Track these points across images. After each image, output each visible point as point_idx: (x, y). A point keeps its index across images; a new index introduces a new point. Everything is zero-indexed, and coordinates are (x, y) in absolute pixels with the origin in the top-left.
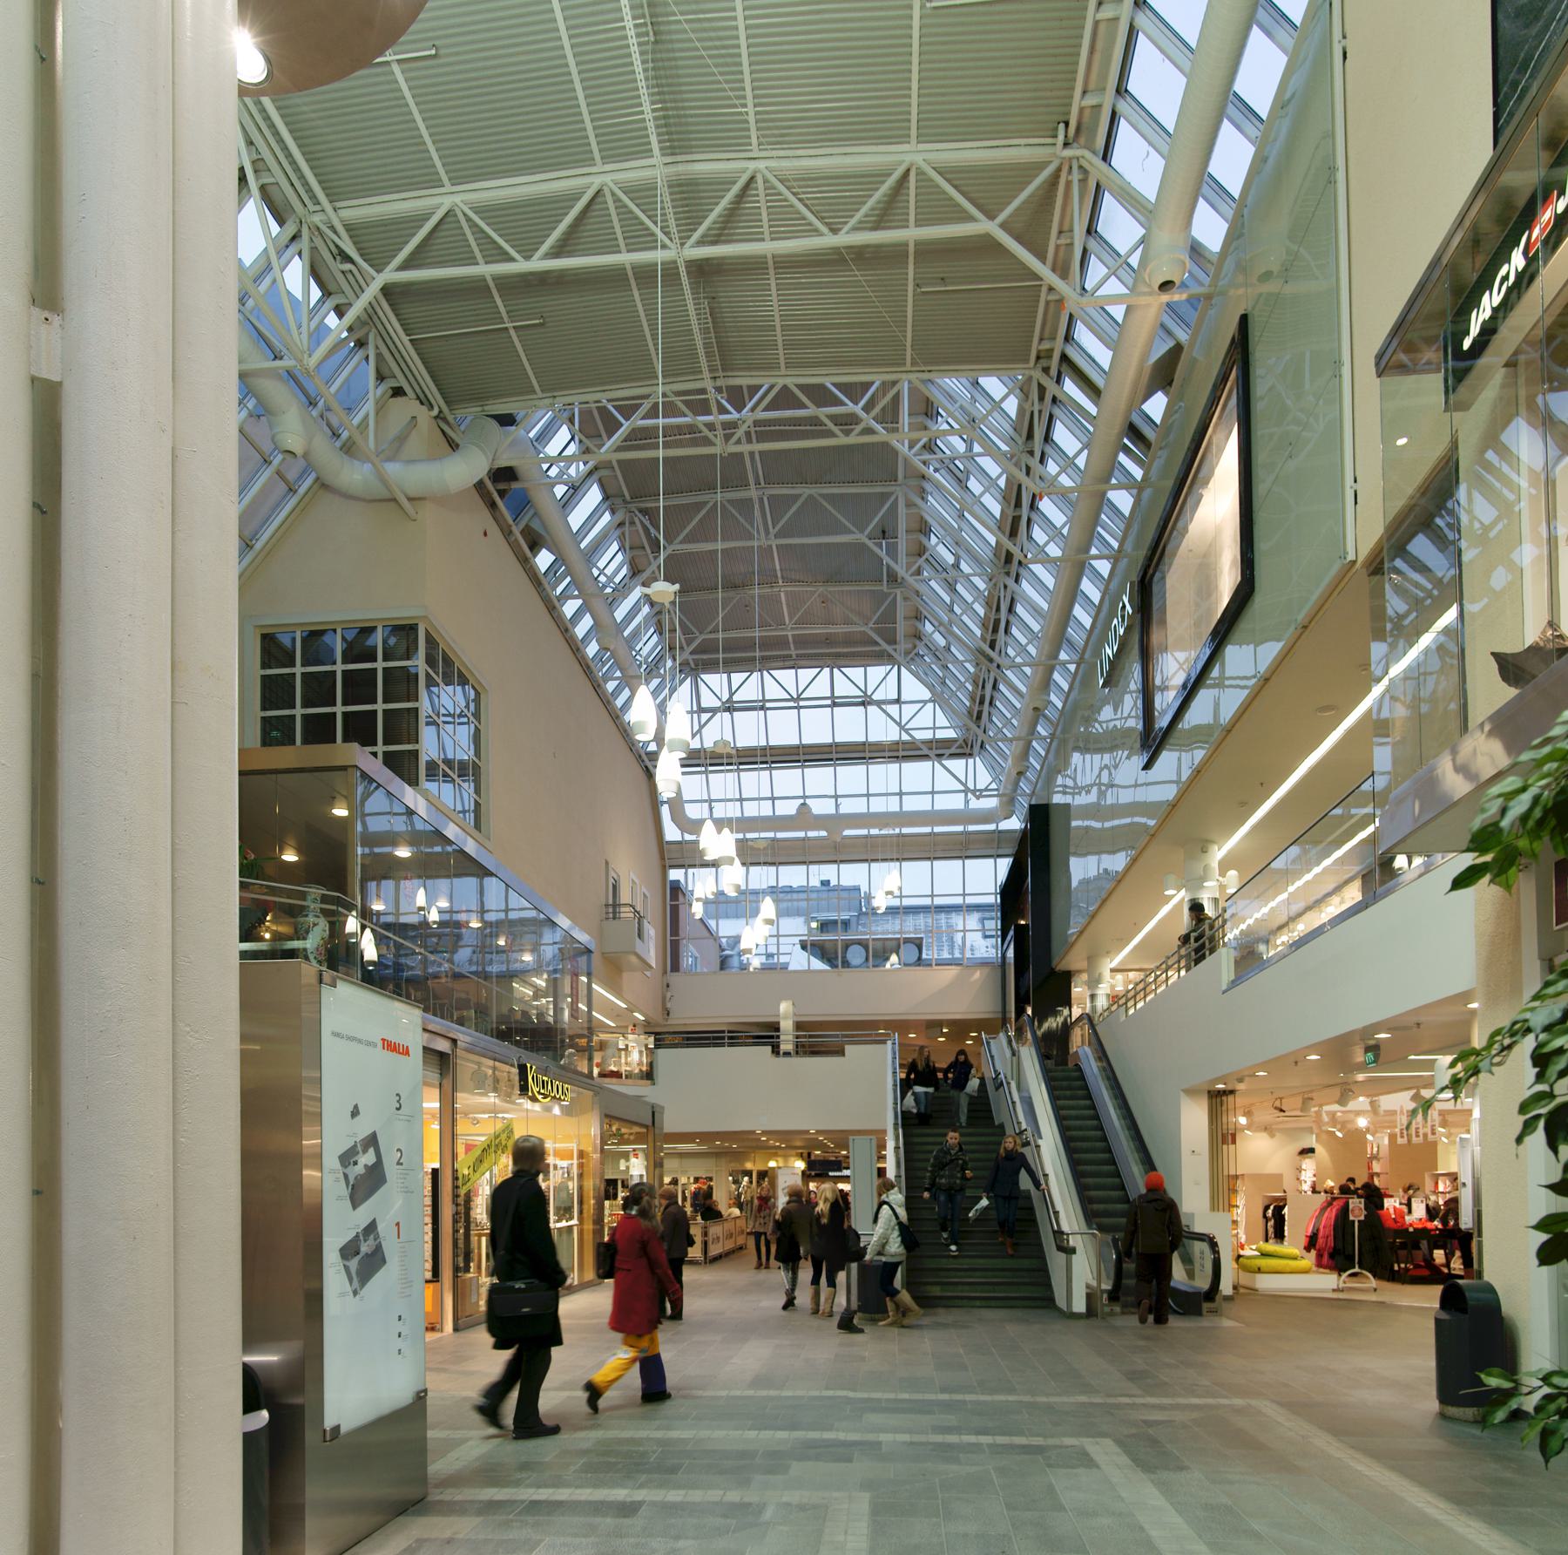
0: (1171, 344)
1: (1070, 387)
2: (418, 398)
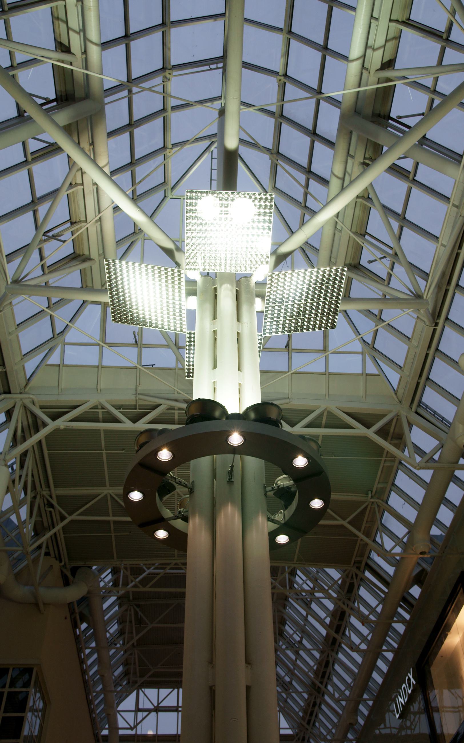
0: (420, 569)
1: (367, 574)
2: (55, 557)
